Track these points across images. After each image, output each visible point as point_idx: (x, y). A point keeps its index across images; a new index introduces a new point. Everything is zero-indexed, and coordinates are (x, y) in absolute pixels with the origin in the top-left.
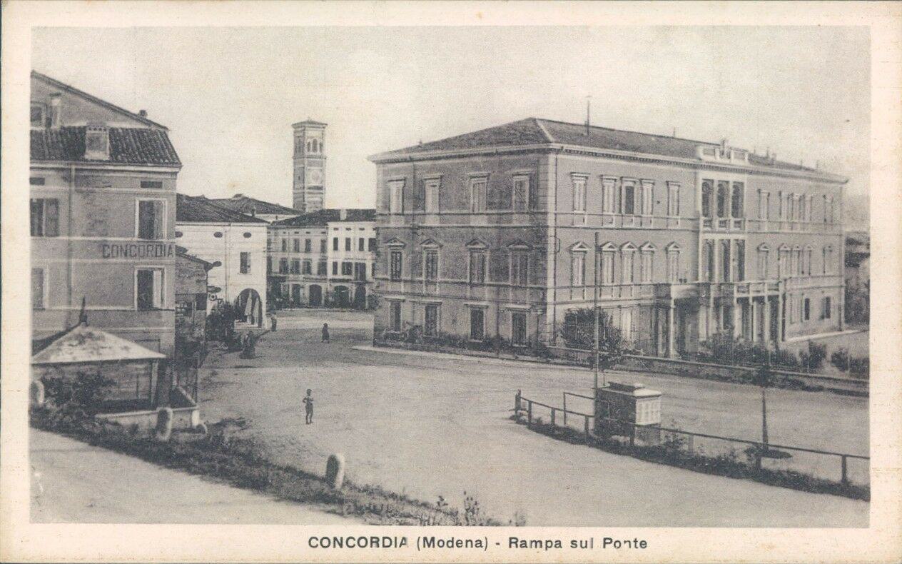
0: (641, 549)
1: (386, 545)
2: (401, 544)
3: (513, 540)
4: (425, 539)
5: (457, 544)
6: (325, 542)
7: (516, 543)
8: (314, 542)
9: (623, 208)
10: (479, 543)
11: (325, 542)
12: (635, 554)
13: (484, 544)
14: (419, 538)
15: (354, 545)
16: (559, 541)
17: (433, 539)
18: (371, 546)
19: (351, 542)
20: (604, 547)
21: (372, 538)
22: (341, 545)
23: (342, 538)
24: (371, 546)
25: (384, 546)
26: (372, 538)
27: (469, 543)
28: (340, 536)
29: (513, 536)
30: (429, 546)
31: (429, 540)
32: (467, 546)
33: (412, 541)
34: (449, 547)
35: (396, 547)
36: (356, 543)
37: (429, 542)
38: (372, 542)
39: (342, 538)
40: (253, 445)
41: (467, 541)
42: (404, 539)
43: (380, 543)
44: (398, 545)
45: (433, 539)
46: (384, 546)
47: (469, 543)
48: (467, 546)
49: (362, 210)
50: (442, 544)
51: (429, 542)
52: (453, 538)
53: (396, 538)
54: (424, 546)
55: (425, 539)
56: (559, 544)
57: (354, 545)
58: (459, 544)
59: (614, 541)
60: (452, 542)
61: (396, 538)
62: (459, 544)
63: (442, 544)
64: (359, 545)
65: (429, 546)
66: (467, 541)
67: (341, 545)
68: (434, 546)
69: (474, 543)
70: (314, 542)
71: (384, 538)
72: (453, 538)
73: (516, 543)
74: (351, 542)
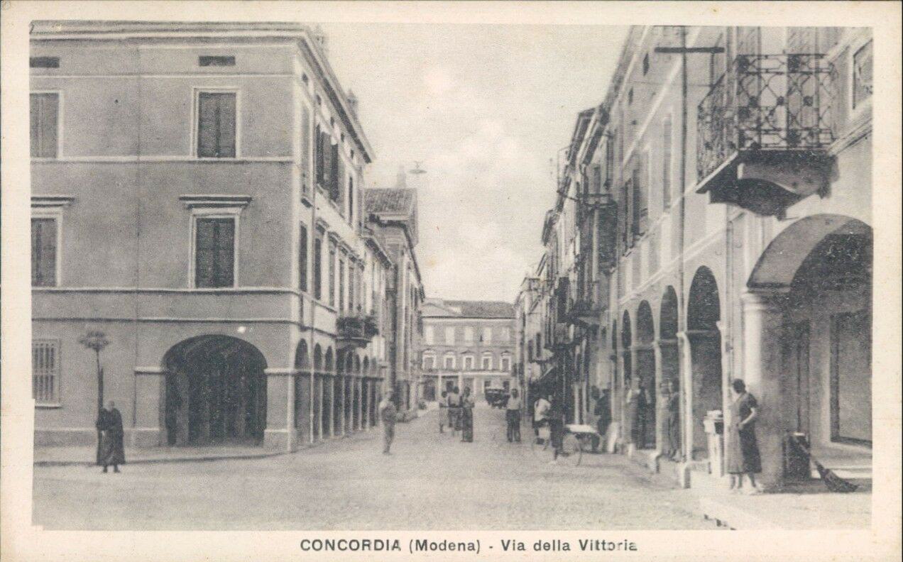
0: (450, 551)
1: (353, 548)
2: (394, 547)
3: (366, 543)
4: (418, 541)
5: (544, 547)
6: (354, 545)
7: (368, 545)
8: (306, 545)
9: (405, 389)
10: (472, 547)
11: (317, 545)
12: (470, 555)
13: (476, 547)
14: (412, 541)
15: (309, 548)
16: (522, 544)
17: (425, 542)
18: (363, 549)
19: (343, 545)
20: (636, 550)
21: (364, 541)
22: (333, 548)
23: (334, 541)
24: (363, 549)
25: (376, 549)
26: (364, 541)
27: (462, 546)
28: (333, 538)
29: (366, 538)
30: (421, 549)
31: (422, 543)
32: (459, 549)
33: (404, 544)
34: (442, 550)
35: (388, 549)
36: (310, 545)
37: (422, 545)
38: (364, 545)
39: (334, 541)
40: (391, 420)
41: (459, 544)
42: (397, 542)
43: (372, 546)
44: (390, 548)
45: (425, 542)
46: (376, 549)
47: (462, 546)
48: (459, 549)
49: (35, 367)
50: (435, 546)
51: (422, 545)
52: (540, 541)
53: (388, 541)
54: (417, 549)
55: (418, 541)
56: (522, 547)
57: (309, 548)
58: (452, 546)
59: (348, 541)
60: (540, 545)
61: (388, 541)
62: (452, 546)
63: (435, 546)
64: (314, 548)
65: (421, 549)
66: (459, 544)
67: (333, 548)
68: (426, 549)
69: (467, 546)
70: (306, 545)
71: (376, 541)
72: (540, 541)
73: (368, 545)
74: (343, 545)
